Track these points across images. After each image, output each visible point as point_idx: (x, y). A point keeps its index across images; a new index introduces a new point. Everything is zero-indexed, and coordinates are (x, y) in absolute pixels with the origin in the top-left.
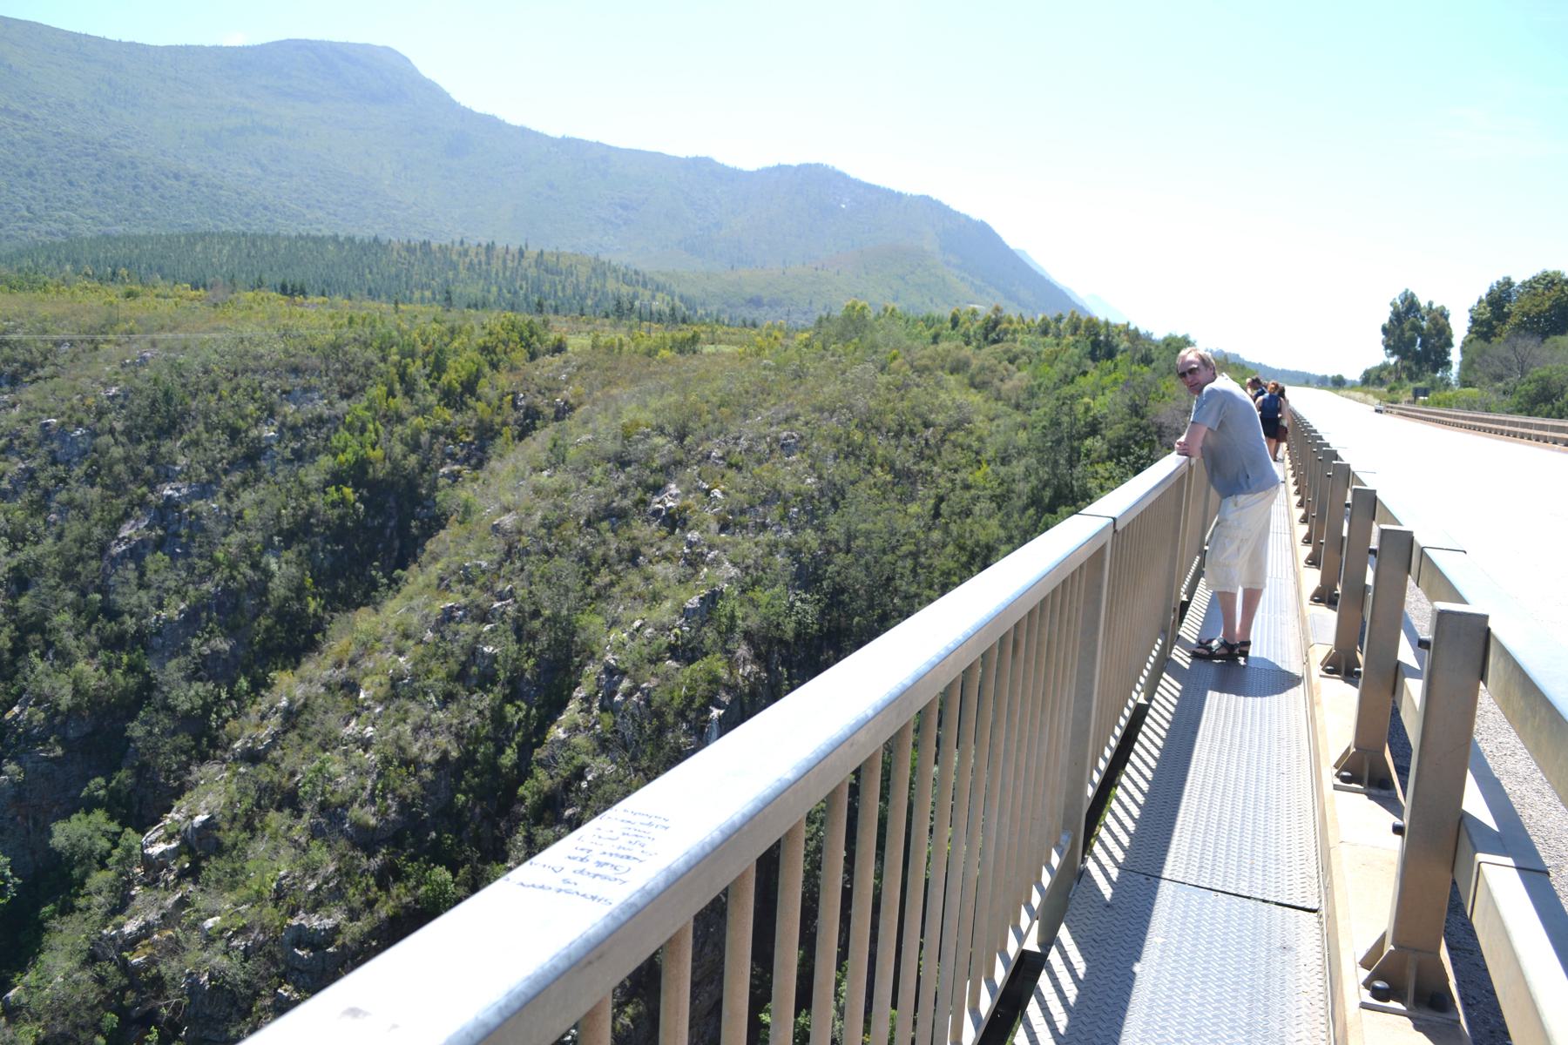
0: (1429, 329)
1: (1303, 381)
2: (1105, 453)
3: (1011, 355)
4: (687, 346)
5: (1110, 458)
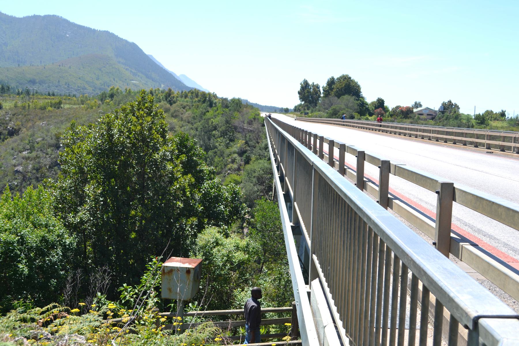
0: (313, 92)
1: (274, 110)
2: (220, 135)
3: (183, 106)
4: (58, 105)
5: (221, 136)
